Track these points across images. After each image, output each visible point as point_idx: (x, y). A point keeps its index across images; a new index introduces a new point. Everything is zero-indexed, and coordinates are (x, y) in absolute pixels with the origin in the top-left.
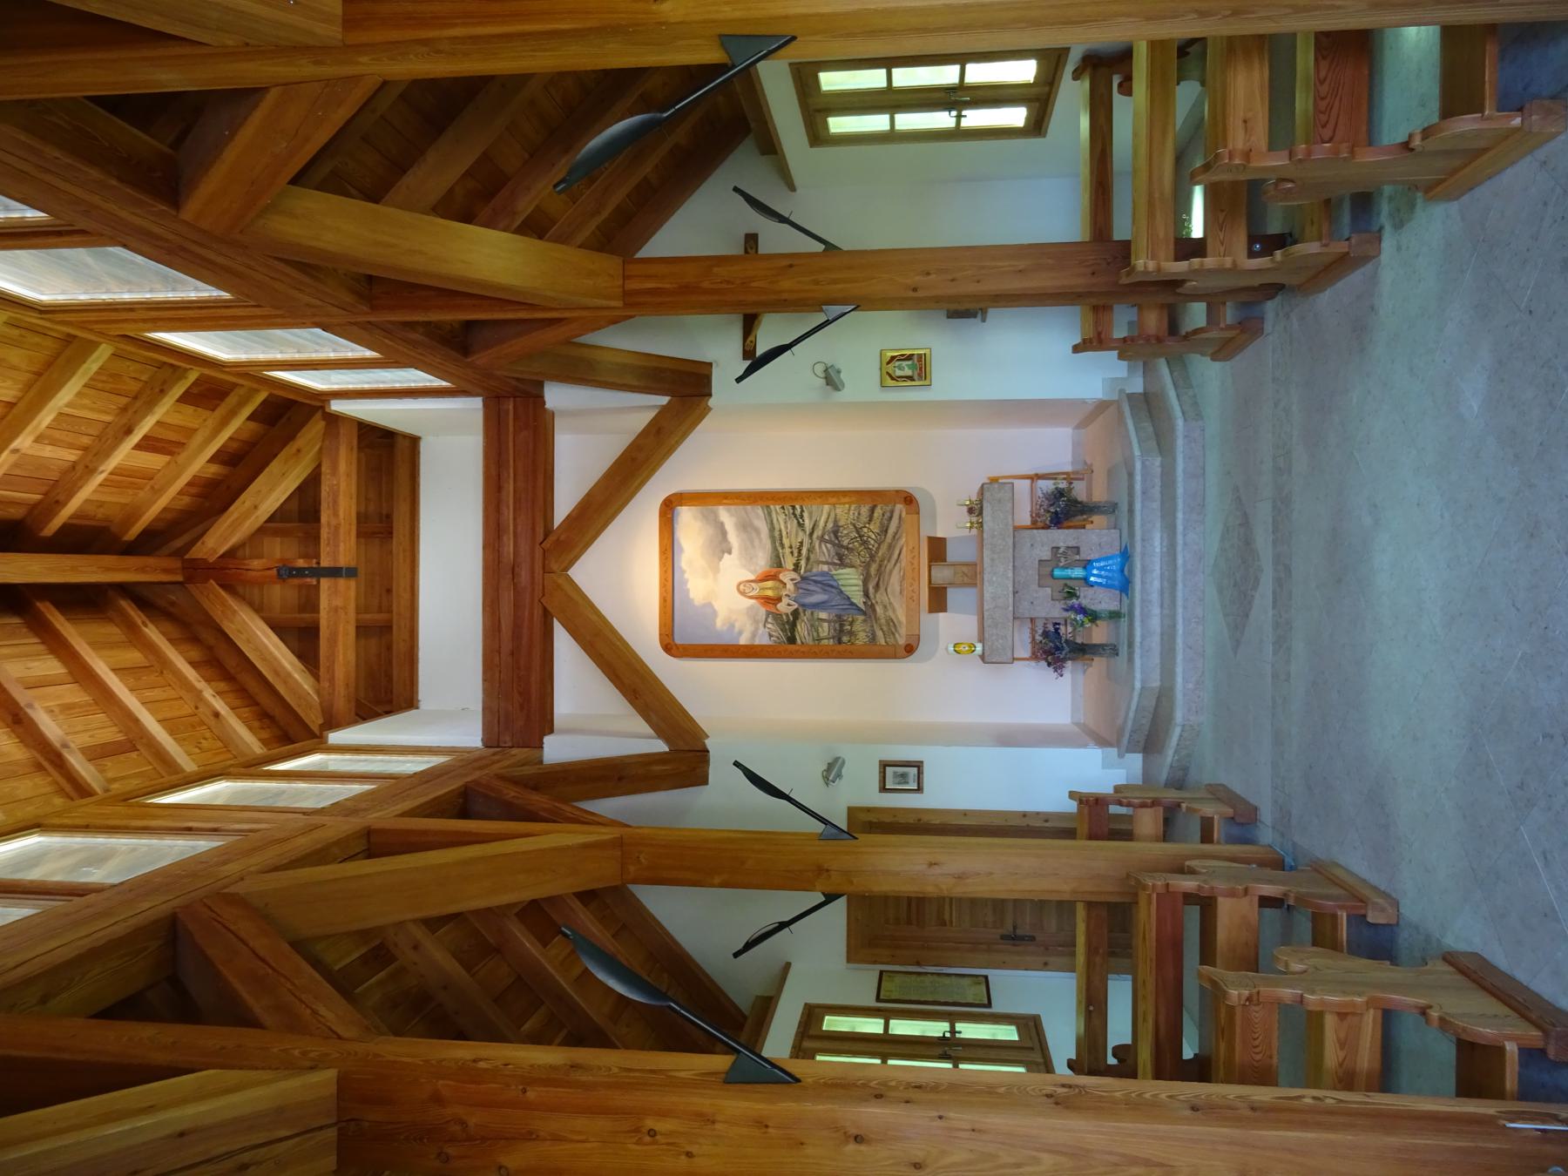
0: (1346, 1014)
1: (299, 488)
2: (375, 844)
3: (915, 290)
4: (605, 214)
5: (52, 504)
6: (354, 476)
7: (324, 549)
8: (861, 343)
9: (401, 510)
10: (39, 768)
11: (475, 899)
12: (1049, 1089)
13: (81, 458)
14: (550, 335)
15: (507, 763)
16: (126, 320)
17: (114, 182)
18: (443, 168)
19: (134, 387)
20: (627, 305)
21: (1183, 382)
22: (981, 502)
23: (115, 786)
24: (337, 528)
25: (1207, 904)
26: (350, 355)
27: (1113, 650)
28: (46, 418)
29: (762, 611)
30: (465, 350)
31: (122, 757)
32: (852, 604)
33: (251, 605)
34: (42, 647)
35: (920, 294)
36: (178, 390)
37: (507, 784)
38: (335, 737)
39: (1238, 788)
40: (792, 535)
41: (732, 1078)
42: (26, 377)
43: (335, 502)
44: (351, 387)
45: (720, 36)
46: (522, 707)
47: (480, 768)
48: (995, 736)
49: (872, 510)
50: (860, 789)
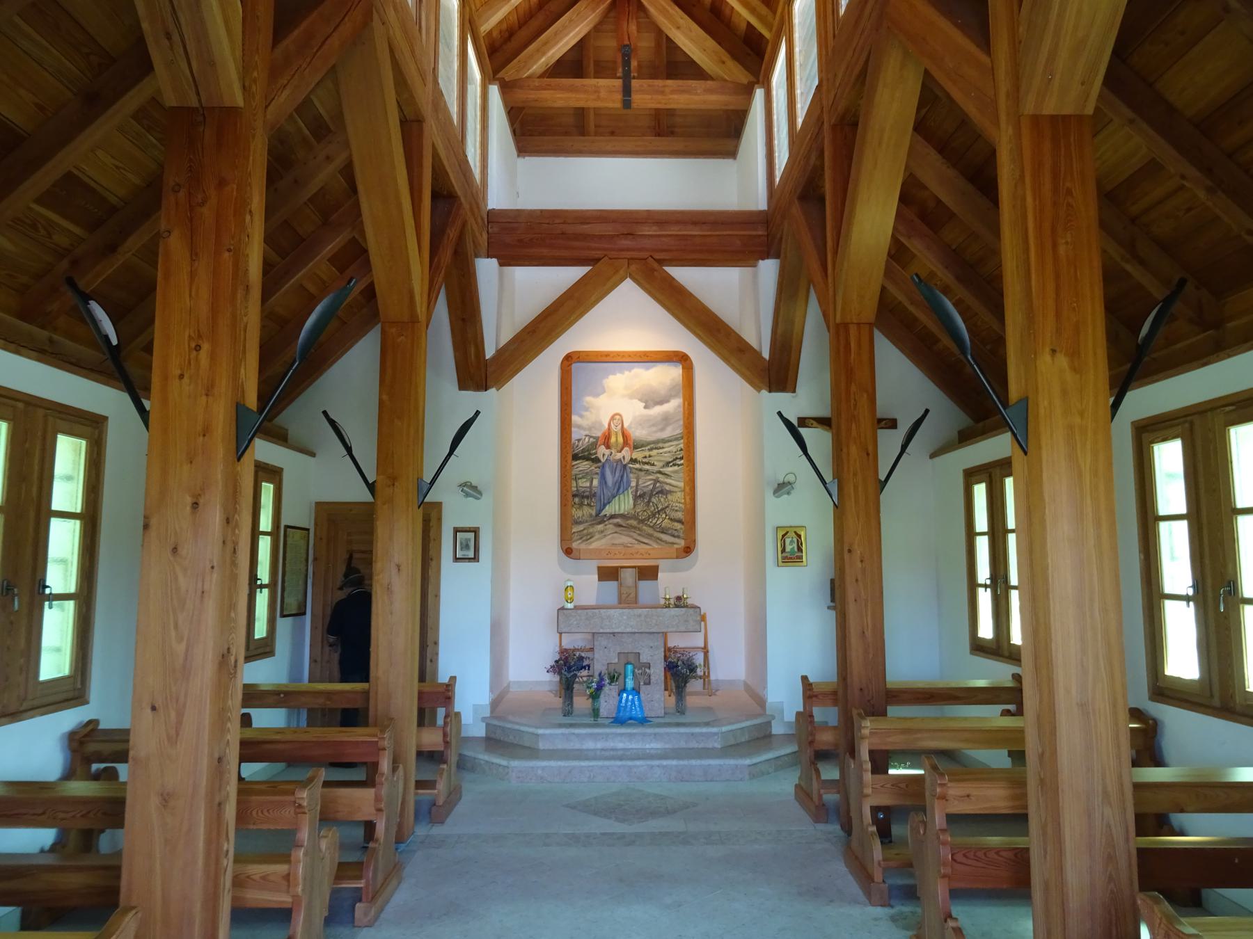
0: (288, 881)
1: (693, 62)
2: (412, 126)
3: (850, 551)
4: (911, 309)
6: (703, 107)
7: (645, 83)
8: (810, 510)
9: (678, 144)
11: (368, 206)
12: (233, 651)
14: (814, 265)
18: (941, 182)
21: (780, 764)
22: (686, 606)
24: (662, 93)
25: (369, 783)
26: (799, 106)
27: (567, 713)
29: (599, 434)
32: (605, 506)
35: (846, 556)
37: (461, 233)
38: (494, 90)
39: (460, 809)
40: (660, 457)
41: (240, 409)
43: (683, 92)
44: (775, 105)
45: (1027, 398)
46: (520, 241)
47: (471, 209)
48: (496, 621)
49: (679, 521)
50: (456, 512)
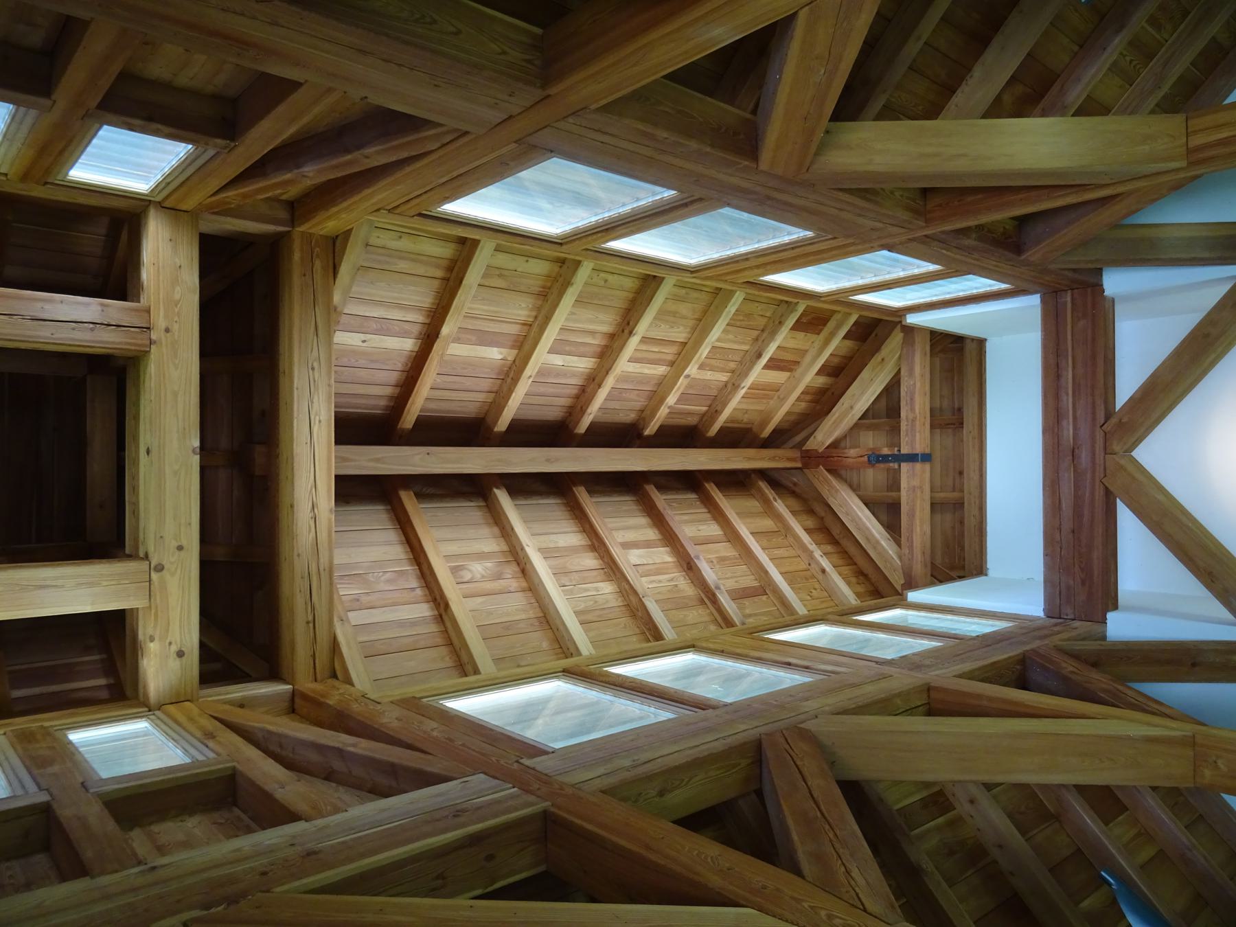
2: (935, 703)
4: (1166, 89)
5: (714, 413)
7: (904, 440)
10: (702, 602)
13: (731, 378)
15: (1065, 635)
16: (745, 269)
17: (708, 149)
19: (763, 321)
20: (1191, 164)
23: (751, 620)
24: (914, 420)
26: (916, 271)
28: (704, 351)
30: (1018, 249)
31: (756, 599)
33: (851, 486)
34: (709, 515)
36: (791, 321)
38: (913, 596)
42: (691, 323)
46: (1083, 583)
